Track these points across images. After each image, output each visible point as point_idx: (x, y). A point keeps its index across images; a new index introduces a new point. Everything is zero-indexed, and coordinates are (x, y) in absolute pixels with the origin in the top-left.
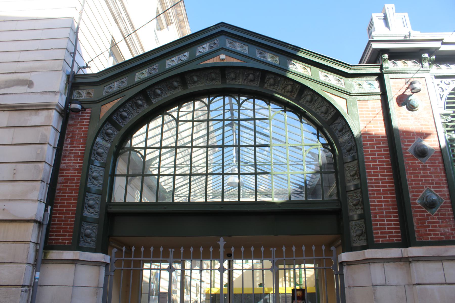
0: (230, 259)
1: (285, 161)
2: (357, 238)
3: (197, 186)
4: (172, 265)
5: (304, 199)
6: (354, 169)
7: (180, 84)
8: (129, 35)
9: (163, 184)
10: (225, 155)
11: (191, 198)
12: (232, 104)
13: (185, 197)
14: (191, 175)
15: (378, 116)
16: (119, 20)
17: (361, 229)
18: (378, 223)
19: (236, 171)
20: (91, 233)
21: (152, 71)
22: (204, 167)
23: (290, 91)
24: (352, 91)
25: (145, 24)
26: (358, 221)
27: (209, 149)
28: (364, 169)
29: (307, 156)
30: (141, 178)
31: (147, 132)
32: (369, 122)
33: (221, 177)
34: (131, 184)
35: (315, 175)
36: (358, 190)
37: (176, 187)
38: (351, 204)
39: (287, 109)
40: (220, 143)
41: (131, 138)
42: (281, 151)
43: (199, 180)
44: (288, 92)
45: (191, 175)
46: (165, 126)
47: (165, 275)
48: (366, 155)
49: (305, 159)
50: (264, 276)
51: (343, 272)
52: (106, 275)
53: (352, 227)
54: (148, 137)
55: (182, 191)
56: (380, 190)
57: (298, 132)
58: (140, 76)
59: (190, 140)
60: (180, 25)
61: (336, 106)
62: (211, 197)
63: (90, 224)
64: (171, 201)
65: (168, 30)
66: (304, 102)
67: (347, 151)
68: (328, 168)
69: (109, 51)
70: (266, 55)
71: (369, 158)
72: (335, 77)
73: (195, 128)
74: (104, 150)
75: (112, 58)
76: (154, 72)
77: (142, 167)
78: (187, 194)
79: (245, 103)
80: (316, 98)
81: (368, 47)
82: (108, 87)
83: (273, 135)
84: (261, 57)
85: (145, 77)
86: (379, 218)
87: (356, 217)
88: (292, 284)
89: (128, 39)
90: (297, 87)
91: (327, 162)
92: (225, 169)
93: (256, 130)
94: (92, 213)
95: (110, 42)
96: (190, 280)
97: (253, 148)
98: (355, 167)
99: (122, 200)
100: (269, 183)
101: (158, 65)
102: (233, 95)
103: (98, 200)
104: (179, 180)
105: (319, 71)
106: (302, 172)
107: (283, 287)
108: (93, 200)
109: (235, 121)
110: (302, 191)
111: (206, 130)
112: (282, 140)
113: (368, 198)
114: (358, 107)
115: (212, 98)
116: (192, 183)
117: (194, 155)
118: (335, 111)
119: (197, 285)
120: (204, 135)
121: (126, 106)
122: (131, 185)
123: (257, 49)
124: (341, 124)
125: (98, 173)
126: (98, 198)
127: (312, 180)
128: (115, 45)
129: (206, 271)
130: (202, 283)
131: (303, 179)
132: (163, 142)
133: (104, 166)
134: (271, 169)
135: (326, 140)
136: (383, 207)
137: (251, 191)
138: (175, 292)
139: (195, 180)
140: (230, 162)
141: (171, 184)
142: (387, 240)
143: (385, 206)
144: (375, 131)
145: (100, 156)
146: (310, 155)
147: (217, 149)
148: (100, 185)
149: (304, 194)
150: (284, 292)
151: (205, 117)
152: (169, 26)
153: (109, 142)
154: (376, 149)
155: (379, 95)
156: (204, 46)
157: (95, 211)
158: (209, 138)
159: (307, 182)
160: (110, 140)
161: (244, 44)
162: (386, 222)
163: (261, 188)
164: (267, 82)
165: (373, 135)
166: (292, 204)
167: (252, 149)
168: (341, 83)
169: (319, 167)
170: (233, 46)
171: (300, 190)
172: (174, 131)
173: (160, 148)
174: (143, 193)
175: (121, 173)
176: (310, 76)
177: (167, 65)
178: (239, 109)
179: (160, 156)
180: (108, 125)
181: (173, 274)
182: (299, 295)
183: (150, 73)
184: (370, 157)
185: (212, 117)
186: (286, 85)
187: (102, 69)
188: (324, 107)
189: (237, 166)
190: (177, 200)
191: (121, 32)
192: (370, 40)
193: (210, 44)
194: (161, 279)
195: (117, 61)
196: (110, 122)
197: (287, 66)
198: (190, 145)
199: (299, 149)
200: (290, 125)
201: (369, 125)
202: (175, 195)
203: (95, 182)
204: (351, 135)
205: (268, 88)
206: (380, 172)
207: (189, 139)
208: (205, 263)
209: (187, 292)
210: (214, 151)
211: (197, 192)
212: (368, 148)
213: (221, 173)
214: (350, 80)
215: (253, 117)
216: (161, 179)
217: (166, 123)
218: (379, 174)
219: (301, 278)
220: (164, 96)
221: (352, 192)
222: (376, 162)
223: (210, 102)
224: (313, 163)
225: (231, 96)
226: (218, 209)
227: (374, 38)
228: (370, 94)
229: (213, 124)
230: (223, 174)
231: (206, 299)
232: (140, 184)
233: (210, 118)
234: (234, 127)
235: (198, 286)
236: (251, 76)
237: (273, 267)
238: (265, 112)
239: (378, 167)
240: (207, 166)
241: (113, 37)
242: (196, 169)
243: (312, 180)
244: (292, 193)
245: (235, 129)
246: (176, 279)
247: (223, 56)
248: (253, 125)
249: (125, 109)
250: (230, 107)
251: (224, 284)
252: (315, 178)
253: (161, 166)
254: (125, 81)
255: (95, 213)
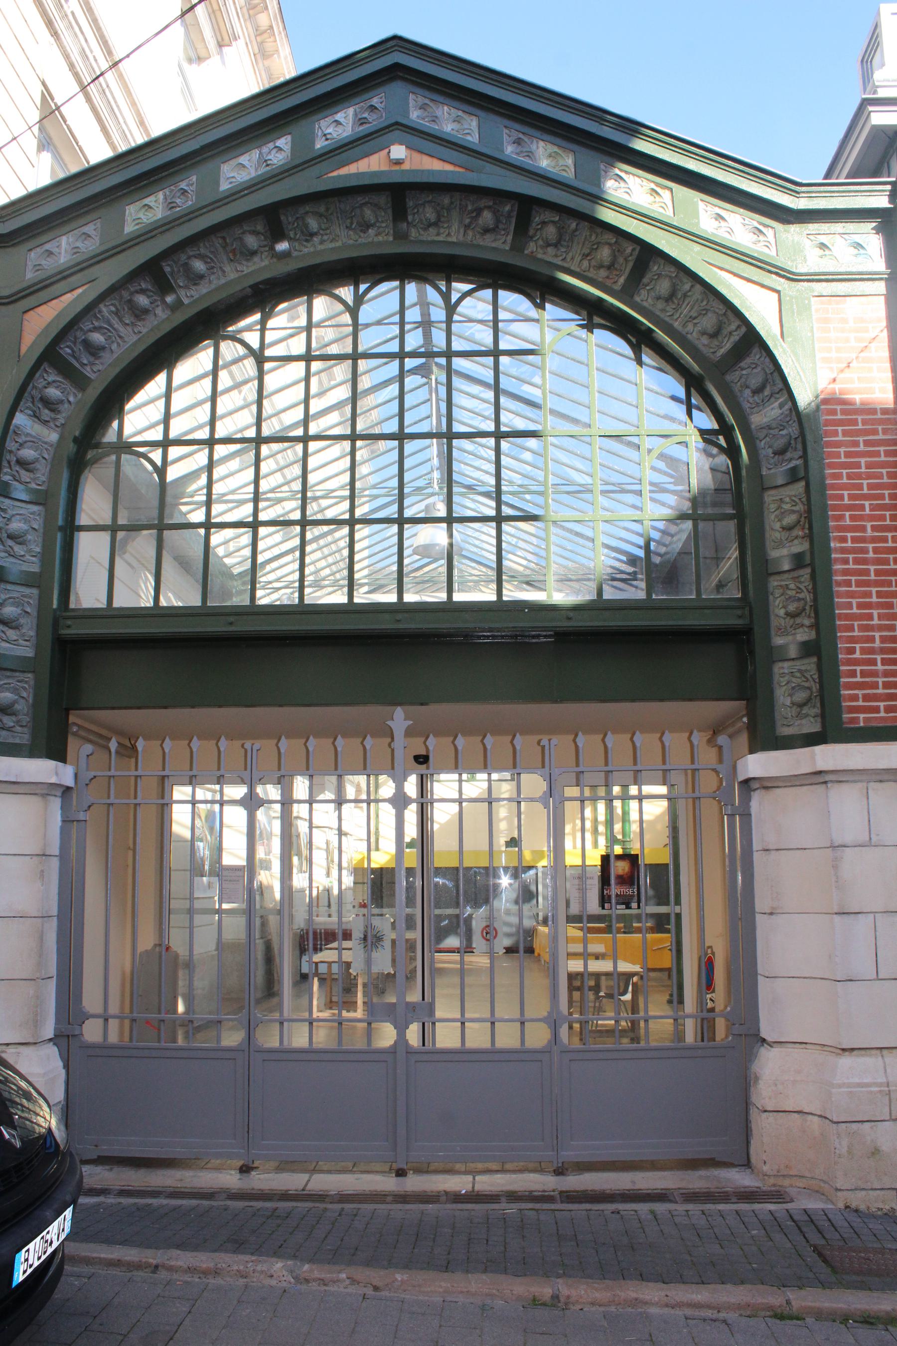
0: (424, 772)
1: (589, 480)
2: (795, 710)
3: (325, 557)
4: (255, 789)
5: (641, 595)
6: (794, 508)
7: (265, 243)
8: (97, 78)
9: (220, 551)
10: (407, 464)
11: (306, 593)
12: (428, 304)
13: (289, 591)
14: (304, 523)
15: (873, 345)
16: (60, 25)
17: (806, 684)
18: (858, 668)
19: (439, 510)
20: (15, 702)
21: (178, 201)
22: (343, 498)
23: (606, 263)
24: (800, 266)
25: (148, 41)
26: (798, 663)
27: (359, 443)
28: (824, 508)
29: (653, 468)
30: (155, 536)
31: (168, 396)
32: (846, 365)
33: (395, 528)
34: (125, 553)
35: (677, 525)
36: (801, 572)
37: (260, 559)
38: (782, 612)
39: (597, 320)
40: (392, 427)
41: (120, 413)
42: (575, 450)
43: (329, 538)
44: (600, 266)
45: (304, 523)
46: (223, 375)
47: (236, 817)
48: (832, 466)
49: (649, 476)
50: (523, 816)
51: (749, 807)
52: (67, 821)
53: (782, 679)
54: (173, 410)
55: (279, 573)
56: (867, 572)
57: (629, 393)
58: (141, 215)
59: (302, 416)
60: (261, 45)
61: (747, 314)
62: (366, 589)
63: (9, 673)
64: (247, 602)
65: (224, 63)
66: (650, 300)
67: (775, 453)
68: (714, 504)
69: (37, 134)
70: (534, 147)
71: (839, 476)
72: (747, 222)
73: (314, 381)
74: (39, 452)
75: (47, 157)
76: (185, 204)
77: (156, 503)
78: (294, 582)
79: (468, 301)
80: (687, 287)
81: (859, 120)
82: (39, 250)
83: (551, 402)
84: (518, 154)
85: (155, 218)
86: (861, 654)
87: (793, 652)
88: (602, 841)
89: (93, 89)
90: (629, 250)
91: (712, 487)
92: (405, 505)
93: (501, 386)
94: (15, 642)
95: (38, 102)
96: (307, 830)
97: (491, 441)
98: (798, 501)
99: (102, 603)
100: (537, 546)
101: (194, 178)
102: (430, 276)
103: (28, 603)
104: (269, 538)
105: (700, 202)
106: (637, 515)
107: (575, 847)
108: (17, 604)
109: (437, 360)
110: (635, 573)
111: (349, 385)
112: (579, 417)
113: (830, 596)
114: (814, 317)
115: (367, 285)
116: (308, 549)
117: (312, 462)
118: (744, 329)
119: (327, 843)
120: (342, 402)
121: (100, 312)
122: (127, 556)
123: (506, 127)
124: (759, 369)
125: (26, 521)
126: (30, 597)
127: (667, 540)
128: (54, 111)
129: (353, 805)
130: (343, 837)
131: (641, 535)
132: (219, 424)
133: (41, 499)
134: (546, 507)
135: (713, 418)
136: (876, 621)
137: (484, 569)
138: (267, 866)
139: (316, 539)
140: (421, 483)
141: (247, 552)
142: (881, 718)
143: (879, 619)
144: (861, 394)
145: (28, 470)
146: (661, 465)
147: (383, 445)
148: (34, 559)
149: (642, 580)
150: (580, 864)
151: (344, 347)
152: (225, 49)
153: (53, 426)
154: (862, 448)
155: (881, 279)
156: (339, 116)
157: (23, 635)
158: (358, 412)
159: (653, 545)
160: (55, 419)
161: (464, 111)
162: (880, 667)
163: (513, 562)
164: (535, 235)
165: (855, 404)
166: (606, 609)
167: (488, 444)
168: (765, 239)
169: (690, 500)
170: (430, 119)
171: (630, 569)
172: (250, 391)
173: (211, 442)
174: (162, 579)
175: (93, 520)
176: (670, 217)
177: (222, 180)
178: (449, 321)
179: (210, 467)
180: (46, 371)
181: (260, 814)
182: (620, 872)
183: (171, 206)
184: (844, 471)
185: (365, 347)
186: (595, 247)
187: (18, 193)
188: (710, 315)
189: (441, 497)
190: (264, 598)
191: (72, 66)
192: (864, 96)
193: (358, 110)
194: (225, 829)
195: (65, 165)
196: (54, 365)
197: (598, 184)
198: (299, 432)
199: (630, 444)
200: (603, 372)
201: (847, 374)
202: (258, 586)
203: (19, 550)
204: (790, 404)
205: (540, 256)
206: (872, 518)
207: (298, 414)
208: (352, 783)
209: (301, 864)
210: (373, 452)
211: (324, 573)
212: (838, 444)
213: (396, 516)
214: (795, 233)
215: (491, 347)
216: (216, 538)
217: (227, 366)
218: (869, 525)
219: (627, 824)
220: (216, 281)
221: (786, 576)
222: (860, 487)
223: (359, 300)
224: (672, 487)
225: (425, 280)
226: (386, 624)
227: (878, 90)
228: (854, 277)
229: (370, 367)
230: (401, 521)
231: (355, 883)
232: (152, 553)
233: (360, 349)
234: (433, 377)
235: (331, 847)
236: (487, 217)
237: (550, 792)
238: (530, 331)
239: (867, 503)
240: (352, 497)
241: (44, 84)
242: (319, 505)
243: (667, 540)
244: (605, 577)
245: (437, 382)
246: (269, 829)
247: (398, 151)
248: (492, 372)
249: (96, 324)
250: (422, 315)
251: (407, 839)
252: (676, 534)
253: (214, 497)
254: (94, 233)
255: (21, 642)
